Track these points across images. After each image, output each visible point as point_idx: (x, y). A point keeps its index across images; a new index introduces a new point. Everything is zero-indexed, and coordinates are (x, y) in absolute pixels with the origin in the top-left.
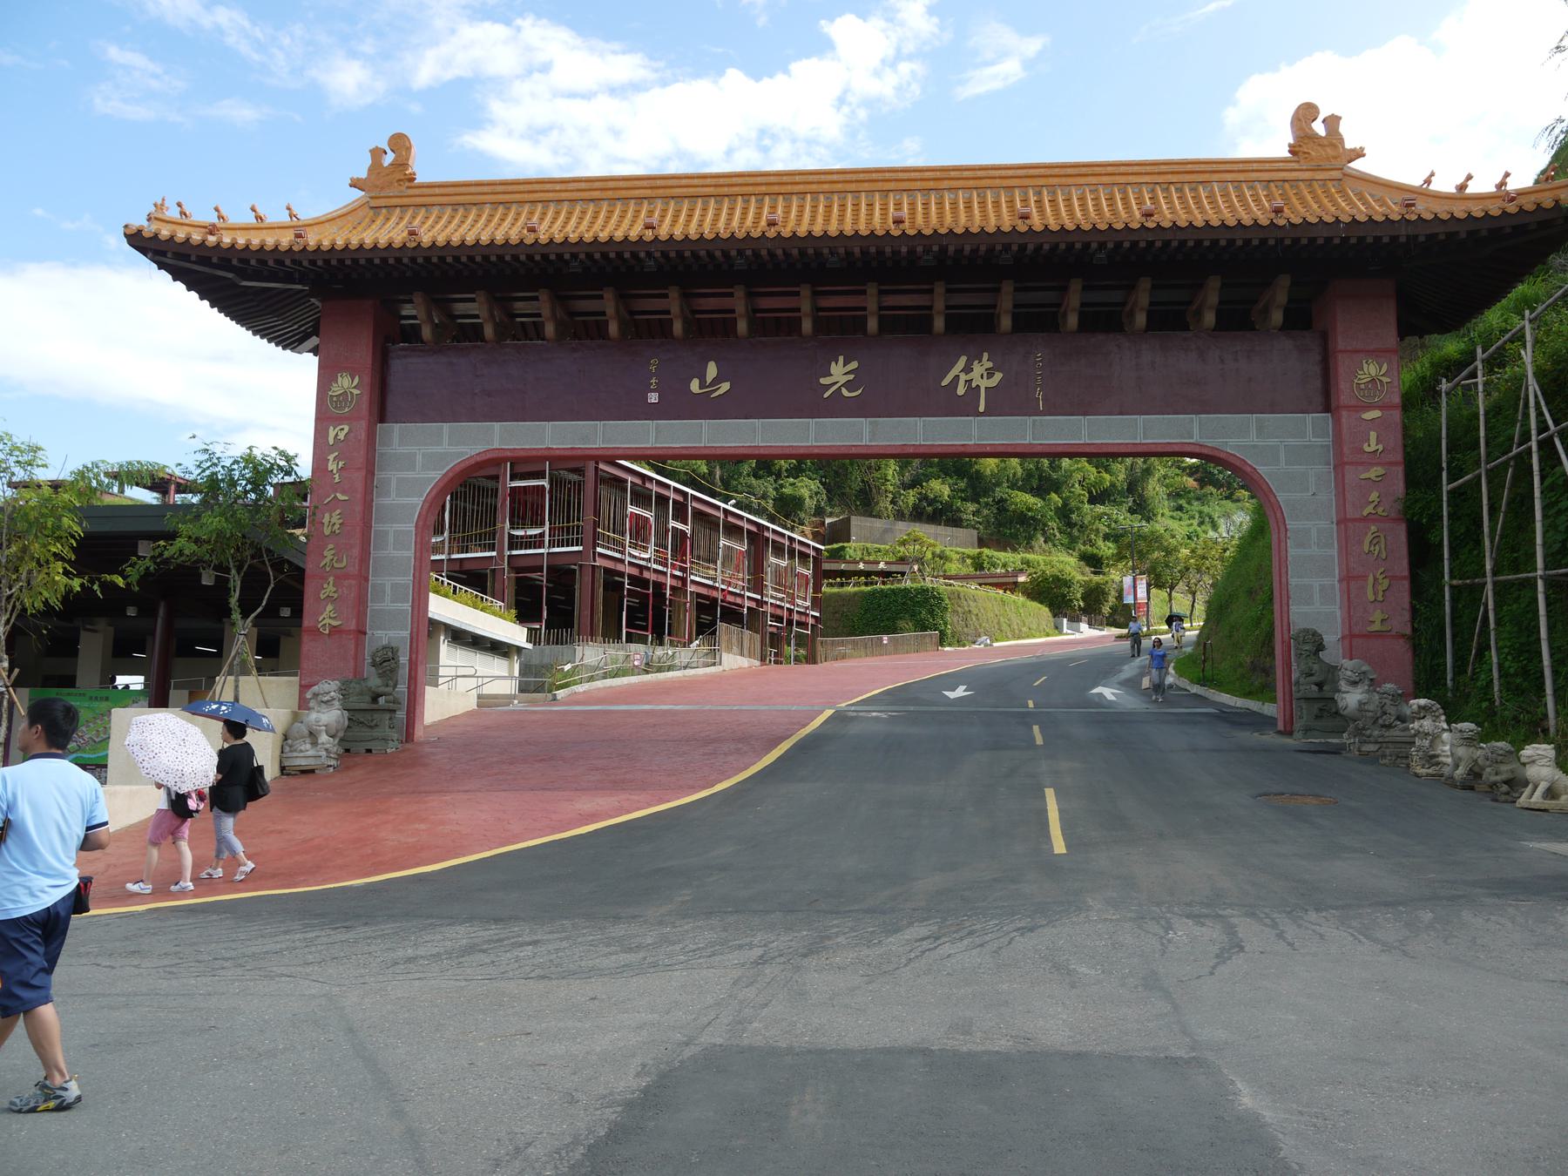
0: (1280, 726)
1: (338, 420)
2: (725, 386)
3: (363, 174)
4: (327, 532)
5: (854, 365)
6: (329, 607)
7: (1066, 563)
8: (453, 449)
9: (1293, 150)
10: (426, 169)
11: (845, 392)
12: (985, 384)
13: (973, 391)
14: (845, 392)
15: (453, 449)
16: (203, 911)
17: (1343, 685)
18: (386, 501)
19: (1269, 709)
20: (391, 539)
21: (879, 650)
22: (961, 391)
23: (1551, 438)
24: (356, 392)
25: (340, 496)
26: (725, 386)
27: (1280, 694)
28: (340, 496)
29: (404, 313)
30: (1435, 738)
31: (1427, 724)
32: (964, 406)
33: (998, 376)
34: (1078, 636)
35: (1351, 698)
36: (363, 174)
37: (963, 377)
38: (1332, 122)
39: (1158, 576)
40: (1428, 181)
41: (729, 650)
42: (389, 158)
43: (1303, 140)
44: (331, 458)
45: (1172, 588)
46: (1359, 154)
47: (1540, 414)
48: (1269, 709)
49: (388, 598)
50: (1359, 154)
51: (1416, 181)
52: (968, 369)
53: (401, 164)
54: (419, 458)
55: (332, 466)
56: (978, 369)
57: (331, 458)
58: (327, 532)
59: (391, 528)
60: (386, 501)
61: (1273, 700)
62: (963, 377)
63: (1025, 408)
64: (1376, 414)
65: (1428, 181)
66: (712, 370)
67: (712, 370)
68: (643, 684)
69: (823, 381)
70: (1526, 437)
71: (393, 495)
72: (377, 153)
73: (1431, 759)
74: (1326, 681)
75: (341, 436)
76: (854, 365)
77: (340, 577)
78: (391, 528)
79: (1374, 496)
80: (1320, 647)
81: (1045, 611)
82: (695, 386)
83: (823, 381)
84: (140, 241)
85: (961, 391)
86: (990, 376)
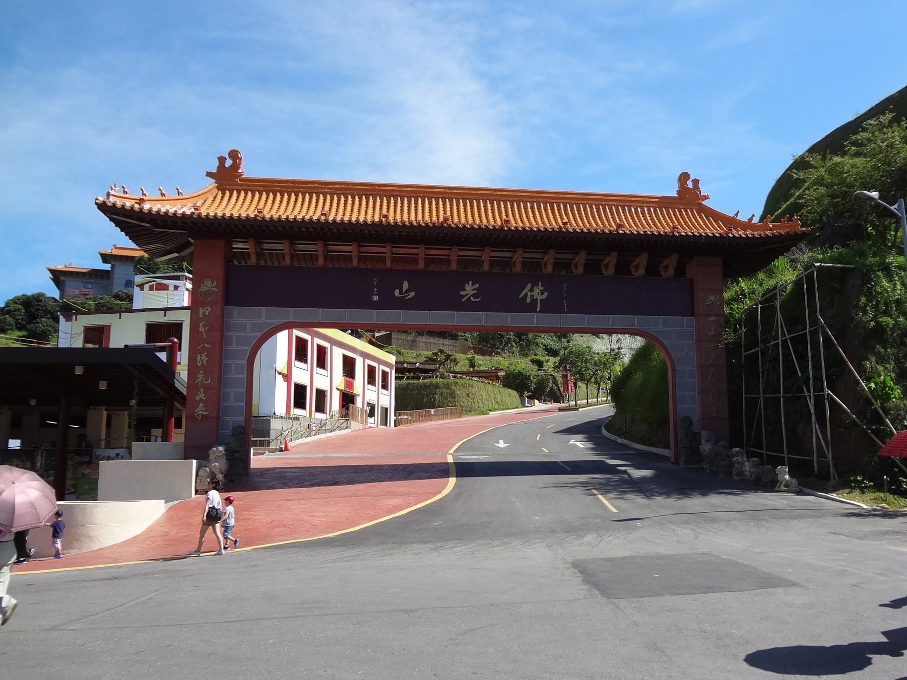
0: (672, 460)
1: (204, 304)
2: (412, 294)
3: (215, 170)
4: (199, 364)
5: (477, 286)
6: (201, 405)
7: (523, 364)
8: (269, 321)
9: (679, 192)
10: (249, 170)
11: (472, 299)
12: (540, 297)
13: (534, 301)
14: (472, 299)
15: (269, 321)
16: (294, 547)
17: (703, 442)
18: (231, 348)
19: (666, 452)
20: (233, 369)
21: (429, 417)
22: (528, 300)
23: (786, 340)
24: (215, 289)
25: (206, 345)
26: (412, 294)
27: (672, 445)
28: (206, 345)
29: (234, 246)
30: (743, 464)
31: (739, 458)
32: (530, 308)
33: (546, 294)
34: (533, 408)
35: (706, 447)
36: (215, 170)
37: (529, 294)
38: (696, 182)
39: (582, 375)
40: (736, 215)
41: (356, 421)
42: (229, 163)
43: (683, 189)
44: (201, 324)
45: (588, 381)
46: (706, 198)
47: (782, 326)
48: (666, 452)
49: (232, 400)
50: (706, 198)
51: (732, 215)
52: (532, 290)
53: (236, 166)
54: (249, 325)
55: (201, 329)
56: (537, 290)
57: (201, 324)
58: (199, 364)
59: (233, 362)
60: (231, 348)
61: (669, 448)
62: (529, 294)
63: (560, 310)
64: (714, 318)
65: (736, 215)
66: (406, 285)
67: (406, 285)
68: (329, 438)
69: (462, 293)
70: (776, 338)
71: (234, 344)
72: (222, 160)
73: (741, 473)
74: (693, 440)
75: (207, 313)
76: (477, 286)
77: (207, 389)
78: (233, 362)
79: (713, 356)
80: (691, 424)
81: (514, 393)
82: (397, 293)
83: (462, 293)
84: (103, 207)
85: (528, 300)
86: (542, 294)
